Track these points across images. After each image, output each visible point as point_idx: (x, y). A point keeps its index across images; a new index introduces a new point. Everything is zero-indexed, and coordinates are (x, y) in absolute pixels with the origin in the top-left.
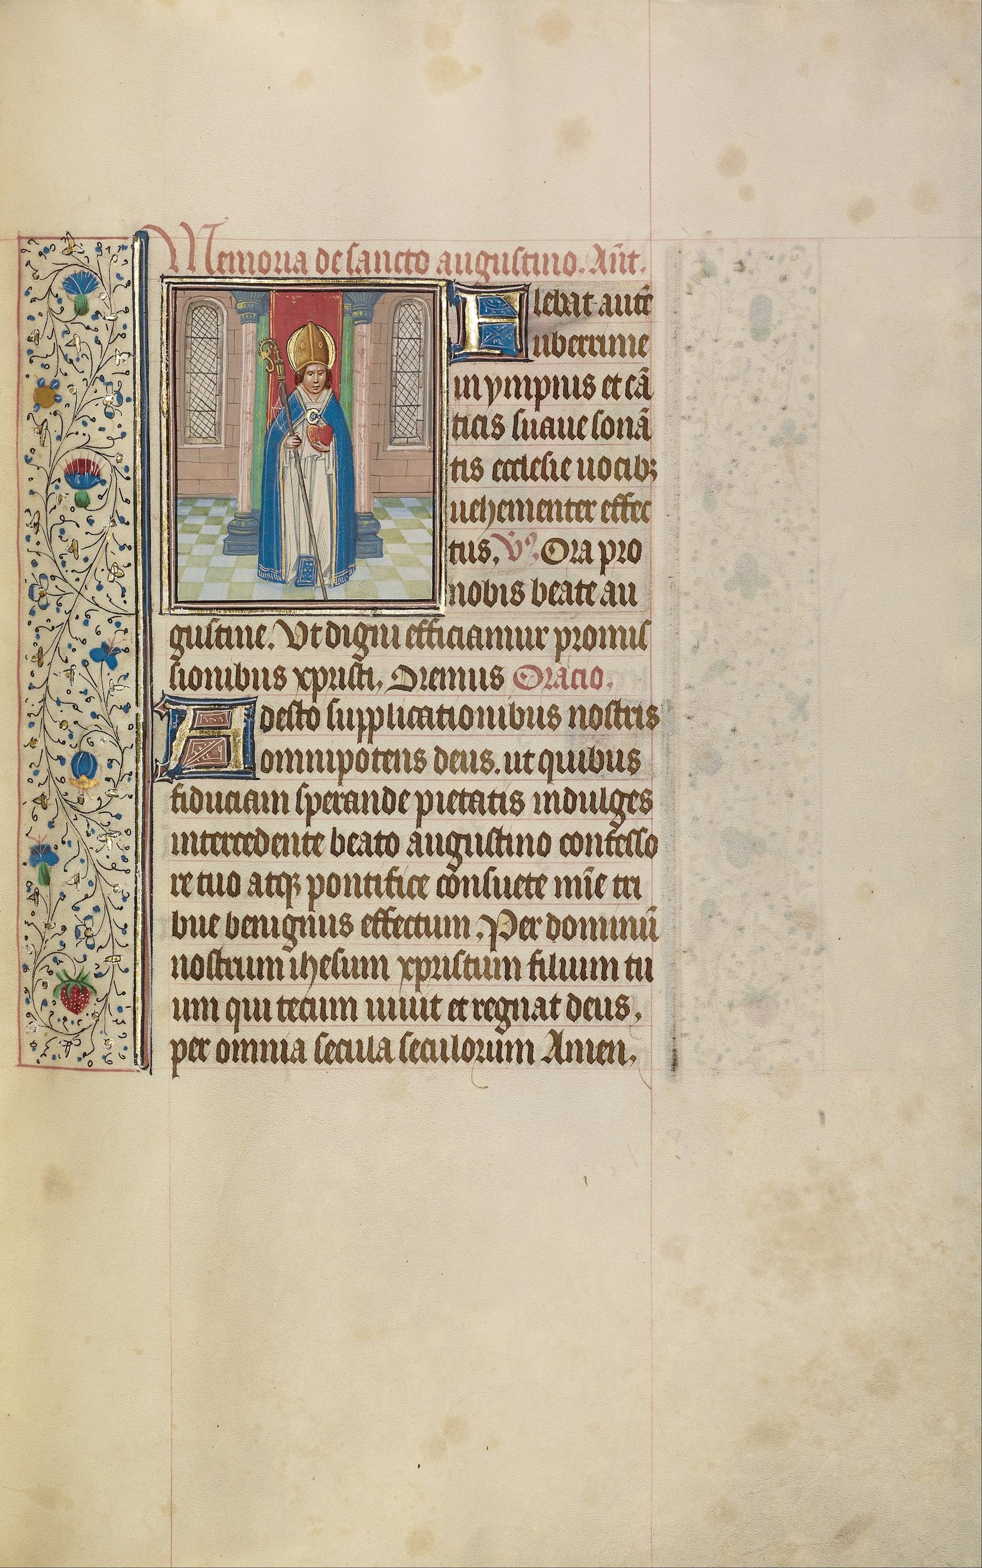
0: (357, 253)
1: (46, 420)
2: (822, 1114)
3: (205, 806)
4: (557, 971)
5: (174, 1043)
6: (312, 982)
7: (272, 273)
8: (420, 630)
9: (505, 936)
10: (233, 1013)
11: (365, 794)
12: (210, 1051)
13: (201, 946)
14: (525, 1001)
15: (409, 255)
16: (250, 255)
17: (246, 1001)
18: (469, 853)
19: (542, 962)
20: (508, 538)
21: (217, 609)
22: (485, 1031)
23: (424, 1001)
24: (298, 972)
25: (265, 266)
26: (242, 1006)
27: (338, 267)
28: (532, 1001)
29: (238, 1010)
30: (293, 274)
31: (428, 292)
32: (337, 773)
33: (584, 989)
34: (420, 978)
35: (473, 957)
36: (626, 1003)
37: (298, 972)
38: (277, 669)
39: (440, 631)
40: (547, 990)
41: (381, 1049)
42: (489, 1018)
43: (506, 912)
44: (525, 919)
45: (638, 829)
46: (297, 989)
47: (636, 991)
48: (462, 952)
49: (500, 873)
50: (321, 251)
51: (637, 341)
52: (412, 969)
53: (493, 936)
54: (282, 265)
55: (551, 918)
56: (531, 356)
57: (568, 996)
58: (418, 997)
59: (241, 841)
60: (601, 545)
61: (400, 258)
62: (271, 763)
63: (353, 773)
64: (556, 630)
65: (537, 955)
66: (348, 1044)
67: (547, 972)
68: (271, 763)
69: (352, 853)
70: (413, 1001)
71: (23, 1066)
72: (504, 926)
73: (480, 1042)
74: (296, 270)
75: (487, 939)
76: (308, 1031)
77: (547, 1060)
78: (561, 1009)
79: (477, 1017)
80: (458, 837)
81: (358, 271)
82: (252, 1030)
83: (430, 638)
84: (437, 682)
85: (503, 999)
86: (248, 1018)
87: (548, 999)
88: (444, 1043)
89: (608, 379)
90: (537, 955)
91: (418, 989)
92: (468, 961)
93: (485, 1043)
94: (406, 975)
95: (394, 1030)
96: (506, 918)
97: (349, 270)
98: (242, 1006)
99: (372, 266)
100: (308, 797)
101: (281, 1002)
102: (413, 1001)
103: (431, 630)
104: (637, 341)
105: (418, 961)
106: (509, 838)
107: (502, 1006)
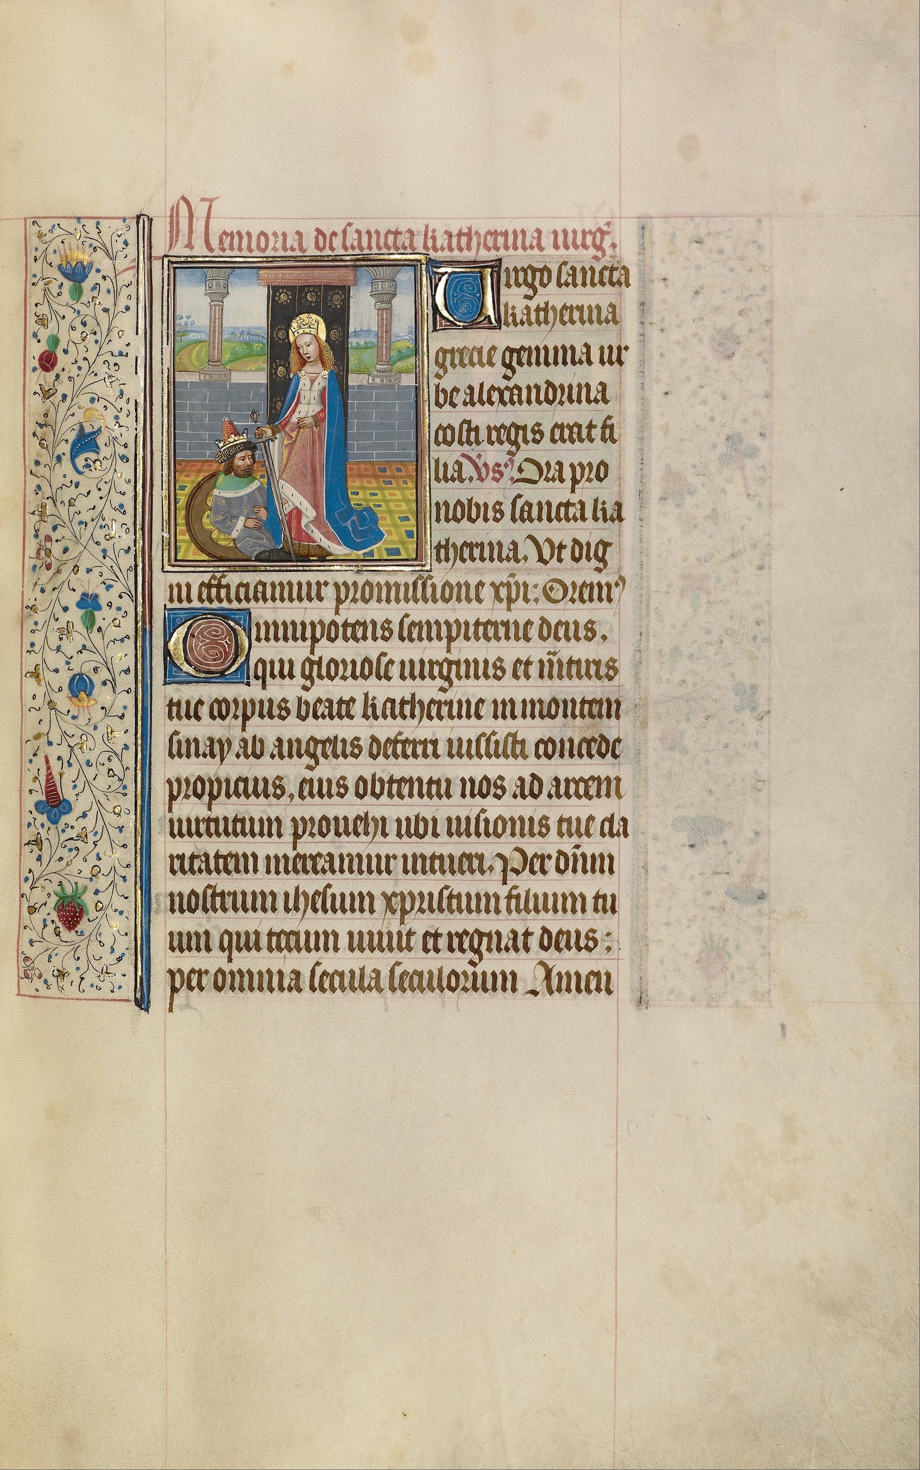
2: (783, 1027)
5: (171, 972)
6: (303, 916)
8: (209, 586)
9: (517, 872)
10: (226, 944)
13: (198, 883)
14: (499, 934)
16: (378, 233)
19: (518, 897)
20: (477, 460)
21: (270, 566)
22: (459, 962)
25: (263, 245)
27: (334, 245)
28: (505, 933)
29: (230, 942)
32: (445, 641)
33: (555, 924)
34: (404, 912)
38: (587, 623)
39: (228, 587)
41: (372, 979)
42: (462, 950)
43: (517, 849)
44: (535, 855)
45: (460, 931)
47: (600, 923)
48: (447, 887)
50: (319, 232)
51: (200, 907)
53: (504, 871)
54: (279, 245)
57: (542, 929)
59: (582, 785)
60: (572, 466)
61: (389, 235)
62: (567, 865)
63: (256, 719)
64: (336, 585)
66: (341, 975)
68: (567, 865)
71: (22, 995)
72: (516, 861)
74: (353, 248)
76: (303, 962)
79: (451, 949)
81: (353, 248)
82: (244, 961)
83: (218, 593)
85: (477, 931)
87: (521, 931)
89: (518, 661)
92: (214, 895)
94: (390, 908)
95: (381, 961)
96: (517, 855)
97: (285, 249)
99: (365, 243)
101: (270, 934)
103: (219, 586)
104: (200, 907)
107: (445, 665)
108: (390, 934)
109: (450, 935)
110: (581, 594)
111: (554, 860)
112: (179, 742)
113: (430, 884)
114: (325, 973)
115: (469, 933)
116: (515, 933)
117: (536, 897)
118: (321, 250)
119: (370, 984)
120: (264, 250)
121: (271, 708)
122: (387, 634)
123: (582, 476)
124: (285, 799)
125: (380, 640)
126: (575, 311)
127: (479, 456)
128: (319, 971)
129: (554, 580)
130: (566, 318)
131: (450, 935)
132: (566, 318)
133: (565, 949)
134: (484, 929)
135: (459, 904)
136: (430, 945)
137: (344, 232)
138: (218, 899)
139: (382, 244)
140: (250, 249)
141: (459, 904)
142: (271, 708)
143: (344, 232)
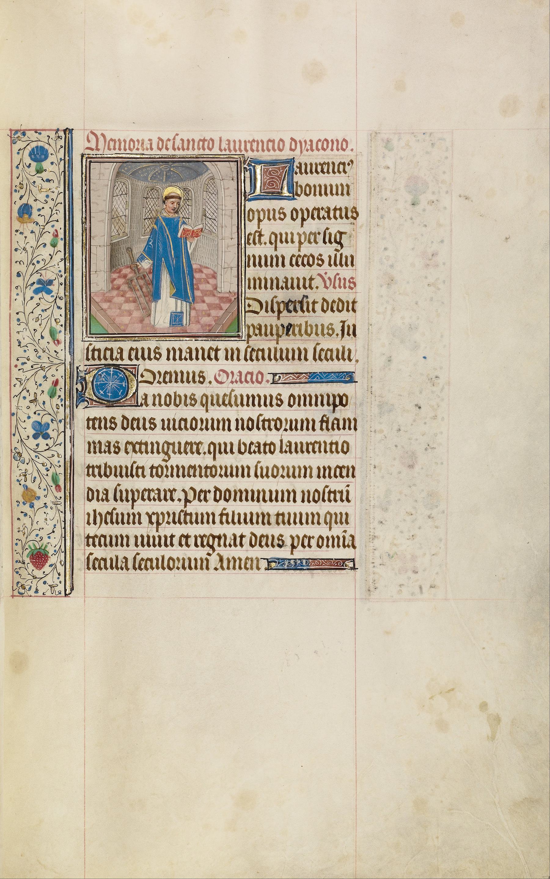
0: (178, 139)
12: (313, 542)
13: (103, 508)
15: (204, 140)
18: (174, 453)
19: (227, 515)
20: (324, 275)
23: (160, 537)
27: (168, 147)
30: (224, 153)
31: (87, 178)
34: (158, 524)
40: (239, 529)
42: (203, 546)
49: (263, 464)
50: (160, 139)
55: (217, 489)
69: (250, 453)
70: (154, 538)
74: (225, 150)
75: (183, 502)
77: (216, 569)
78: (246, 541)
79: (196, 545)
80: (169, 444)
84: (167, 379)
87: (238, 535)
88: (157, 559)
94: (151, 522)
106: (191, 514)
110: (164, 378)
111: (212, 494)
114: (96, 559)
117: (239, 514)
122: (113, 426)
123: (163, 521)
124: (206, 384)
127: (326, 273)
128: (138, 558)
131: (196, 537)
133: (265, 546)
134: (216, 534)
136: (183, 542)
137: (174, 139)
139: (127, 147)
143: (174, 139)
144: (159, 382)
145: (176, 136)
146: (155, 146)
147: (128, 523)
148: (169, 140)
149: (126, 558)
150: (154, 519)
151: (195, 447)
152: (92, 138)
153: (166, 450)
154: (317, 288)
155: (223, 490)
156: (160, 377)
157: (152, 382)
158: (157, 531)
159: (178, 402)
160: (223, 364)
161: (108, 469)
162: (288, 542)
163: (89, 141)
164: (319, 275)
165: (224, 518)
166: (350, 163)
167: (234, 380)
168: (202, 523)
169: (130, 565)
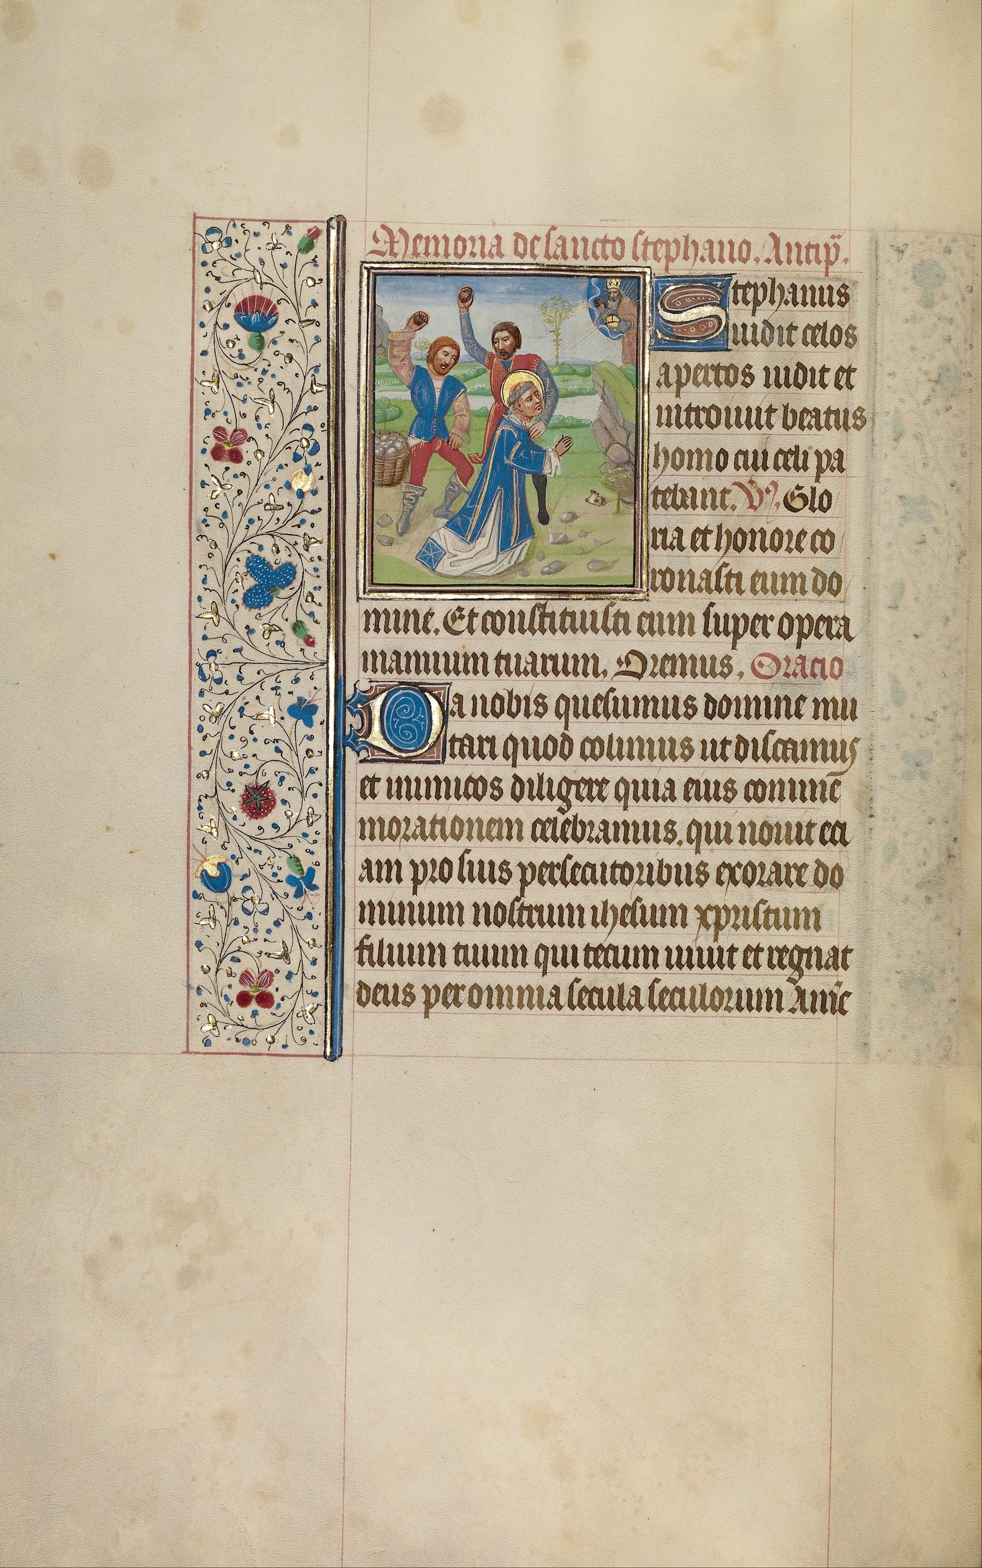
1: (272, 389)
3: (465, 834)
4: (385, 957)
6: (662, 472)
7: (466, 258)
10: (541, 959)
11: (804, 742)
12: (772, 627)
14: (818, 950)
15: (605, 241)
17: (554, 948)
19: (370, 948)
20: (748, 486)
23: (721, 950)
24: (599, 919)
26: (551, 953)
28: (826, 949)
30: (487, 260)
35: (773, 907)
36: (412, 991)
37: (599, 919)
46: (597, 936)
50: (518, 235)
52: (711, 916)
54: (477, 249)
56: (731, 345)
58: (715, 946)
65: (365, 940)
67: (375, 958)
70: (710, 950)
73: (729, 991)
74: (491, 255)
77: (793, 1010)
79: (771, 965)
84: (668, 669)
85: (796, 947)
86: (555, 964)
90: (365, 940)
91: (716, 940)
93: (734, 991)
97: (547, 256)
98: (551, 953)
100: (471, 863)
101: (588, 948)
102: (710, 950)
105: (717, 909)
107: (796, 953)
108: (700, 950)
109: (771, 950)
112: (615, 699)
113: (740, 896)
115: (788, 950)
116: (835, 949)
117: (390, 947)
118: (522, 256)
119: (629, 1003)
120: (461, 256)
121: (396, 994)
123: (727, 922)
124: (733, 677)
125: (497, 882)
126: (710, 370)
128: (658, 987)
129: (633, 652)
130: (700, 378)
132: (700, 378)
135: (600, 999)
136: (751, 960)
137: (548, 236)
138: (525, 913)
140: (447, 254)
141: (600, 999)
142: (396, 994)
143: (548, 236)
144: (653, 674)
145: (552, 232)
146: (507, 247)
147: (561, 924)
148: (537, 238)
149: (637, 989)
150: (711, 916)
151: (595, 789)
152: (382, 234)
153: (564, 793)
154: (734, 508)
155: (831, 866)
156: (655, 665)
157: (640, 672)
158: (716, 940)
159: (514, 709)
160: (633, 641)
161: (665, 871)
162: (420, 995)
163: (376, 240)
164: (740, 485)
165: (366, 953)
166: (771, 488)
167: (790, 671)
168: (561, 924)
169: (563, 999)
